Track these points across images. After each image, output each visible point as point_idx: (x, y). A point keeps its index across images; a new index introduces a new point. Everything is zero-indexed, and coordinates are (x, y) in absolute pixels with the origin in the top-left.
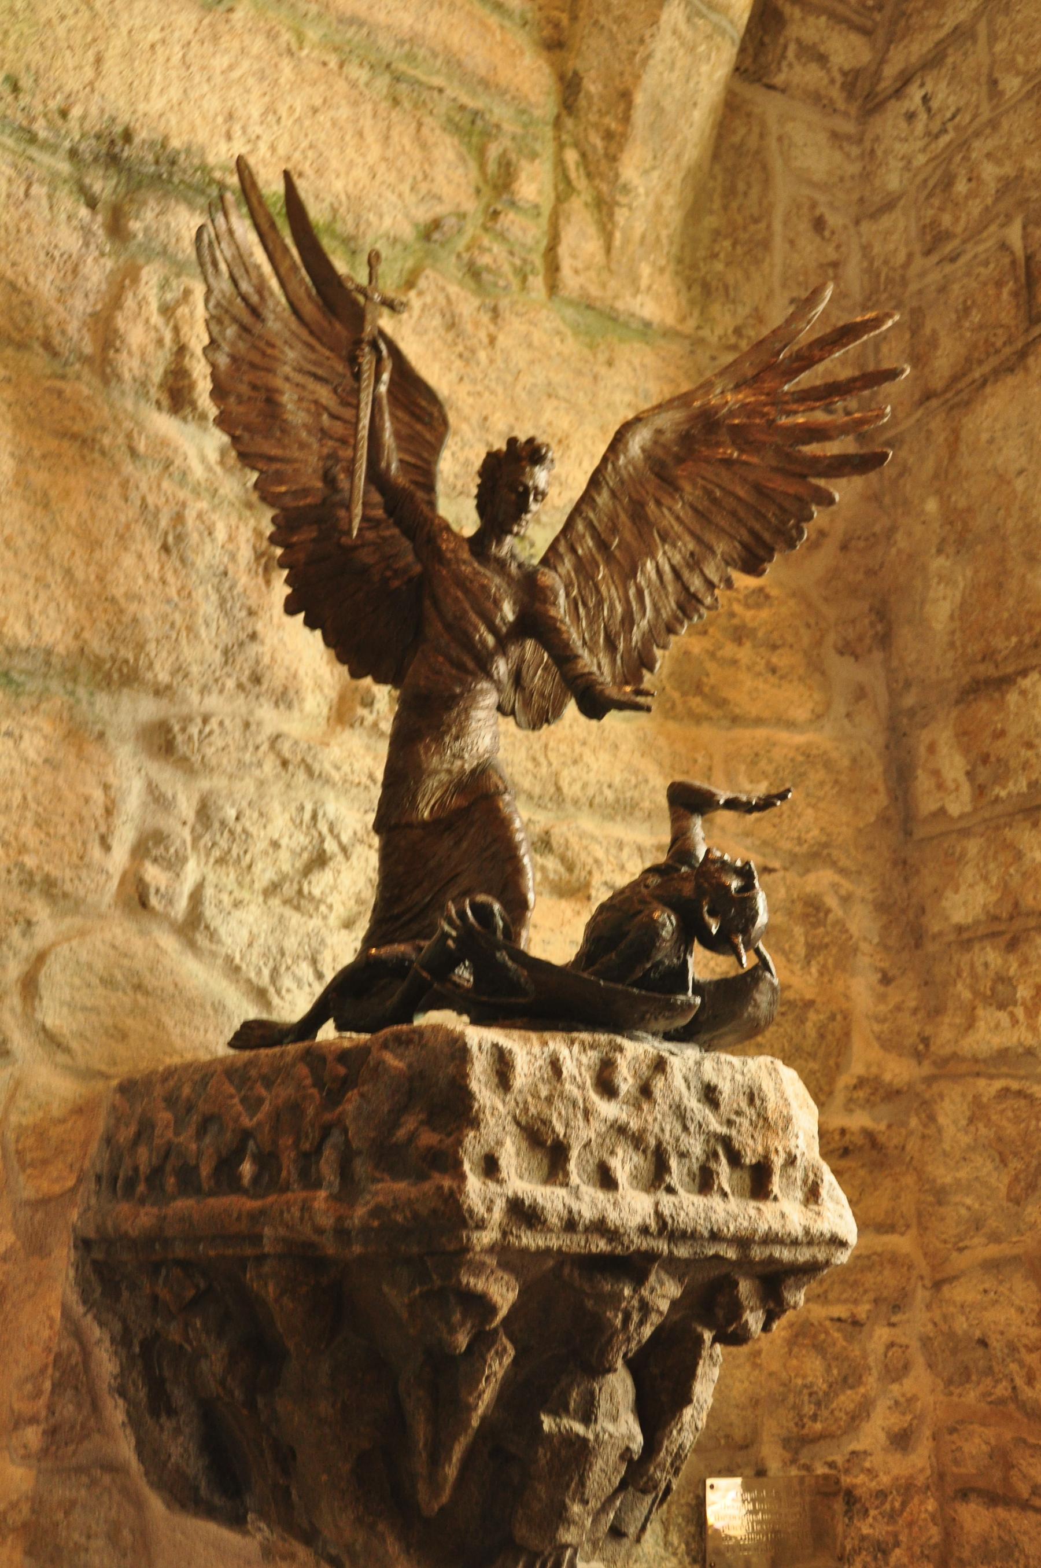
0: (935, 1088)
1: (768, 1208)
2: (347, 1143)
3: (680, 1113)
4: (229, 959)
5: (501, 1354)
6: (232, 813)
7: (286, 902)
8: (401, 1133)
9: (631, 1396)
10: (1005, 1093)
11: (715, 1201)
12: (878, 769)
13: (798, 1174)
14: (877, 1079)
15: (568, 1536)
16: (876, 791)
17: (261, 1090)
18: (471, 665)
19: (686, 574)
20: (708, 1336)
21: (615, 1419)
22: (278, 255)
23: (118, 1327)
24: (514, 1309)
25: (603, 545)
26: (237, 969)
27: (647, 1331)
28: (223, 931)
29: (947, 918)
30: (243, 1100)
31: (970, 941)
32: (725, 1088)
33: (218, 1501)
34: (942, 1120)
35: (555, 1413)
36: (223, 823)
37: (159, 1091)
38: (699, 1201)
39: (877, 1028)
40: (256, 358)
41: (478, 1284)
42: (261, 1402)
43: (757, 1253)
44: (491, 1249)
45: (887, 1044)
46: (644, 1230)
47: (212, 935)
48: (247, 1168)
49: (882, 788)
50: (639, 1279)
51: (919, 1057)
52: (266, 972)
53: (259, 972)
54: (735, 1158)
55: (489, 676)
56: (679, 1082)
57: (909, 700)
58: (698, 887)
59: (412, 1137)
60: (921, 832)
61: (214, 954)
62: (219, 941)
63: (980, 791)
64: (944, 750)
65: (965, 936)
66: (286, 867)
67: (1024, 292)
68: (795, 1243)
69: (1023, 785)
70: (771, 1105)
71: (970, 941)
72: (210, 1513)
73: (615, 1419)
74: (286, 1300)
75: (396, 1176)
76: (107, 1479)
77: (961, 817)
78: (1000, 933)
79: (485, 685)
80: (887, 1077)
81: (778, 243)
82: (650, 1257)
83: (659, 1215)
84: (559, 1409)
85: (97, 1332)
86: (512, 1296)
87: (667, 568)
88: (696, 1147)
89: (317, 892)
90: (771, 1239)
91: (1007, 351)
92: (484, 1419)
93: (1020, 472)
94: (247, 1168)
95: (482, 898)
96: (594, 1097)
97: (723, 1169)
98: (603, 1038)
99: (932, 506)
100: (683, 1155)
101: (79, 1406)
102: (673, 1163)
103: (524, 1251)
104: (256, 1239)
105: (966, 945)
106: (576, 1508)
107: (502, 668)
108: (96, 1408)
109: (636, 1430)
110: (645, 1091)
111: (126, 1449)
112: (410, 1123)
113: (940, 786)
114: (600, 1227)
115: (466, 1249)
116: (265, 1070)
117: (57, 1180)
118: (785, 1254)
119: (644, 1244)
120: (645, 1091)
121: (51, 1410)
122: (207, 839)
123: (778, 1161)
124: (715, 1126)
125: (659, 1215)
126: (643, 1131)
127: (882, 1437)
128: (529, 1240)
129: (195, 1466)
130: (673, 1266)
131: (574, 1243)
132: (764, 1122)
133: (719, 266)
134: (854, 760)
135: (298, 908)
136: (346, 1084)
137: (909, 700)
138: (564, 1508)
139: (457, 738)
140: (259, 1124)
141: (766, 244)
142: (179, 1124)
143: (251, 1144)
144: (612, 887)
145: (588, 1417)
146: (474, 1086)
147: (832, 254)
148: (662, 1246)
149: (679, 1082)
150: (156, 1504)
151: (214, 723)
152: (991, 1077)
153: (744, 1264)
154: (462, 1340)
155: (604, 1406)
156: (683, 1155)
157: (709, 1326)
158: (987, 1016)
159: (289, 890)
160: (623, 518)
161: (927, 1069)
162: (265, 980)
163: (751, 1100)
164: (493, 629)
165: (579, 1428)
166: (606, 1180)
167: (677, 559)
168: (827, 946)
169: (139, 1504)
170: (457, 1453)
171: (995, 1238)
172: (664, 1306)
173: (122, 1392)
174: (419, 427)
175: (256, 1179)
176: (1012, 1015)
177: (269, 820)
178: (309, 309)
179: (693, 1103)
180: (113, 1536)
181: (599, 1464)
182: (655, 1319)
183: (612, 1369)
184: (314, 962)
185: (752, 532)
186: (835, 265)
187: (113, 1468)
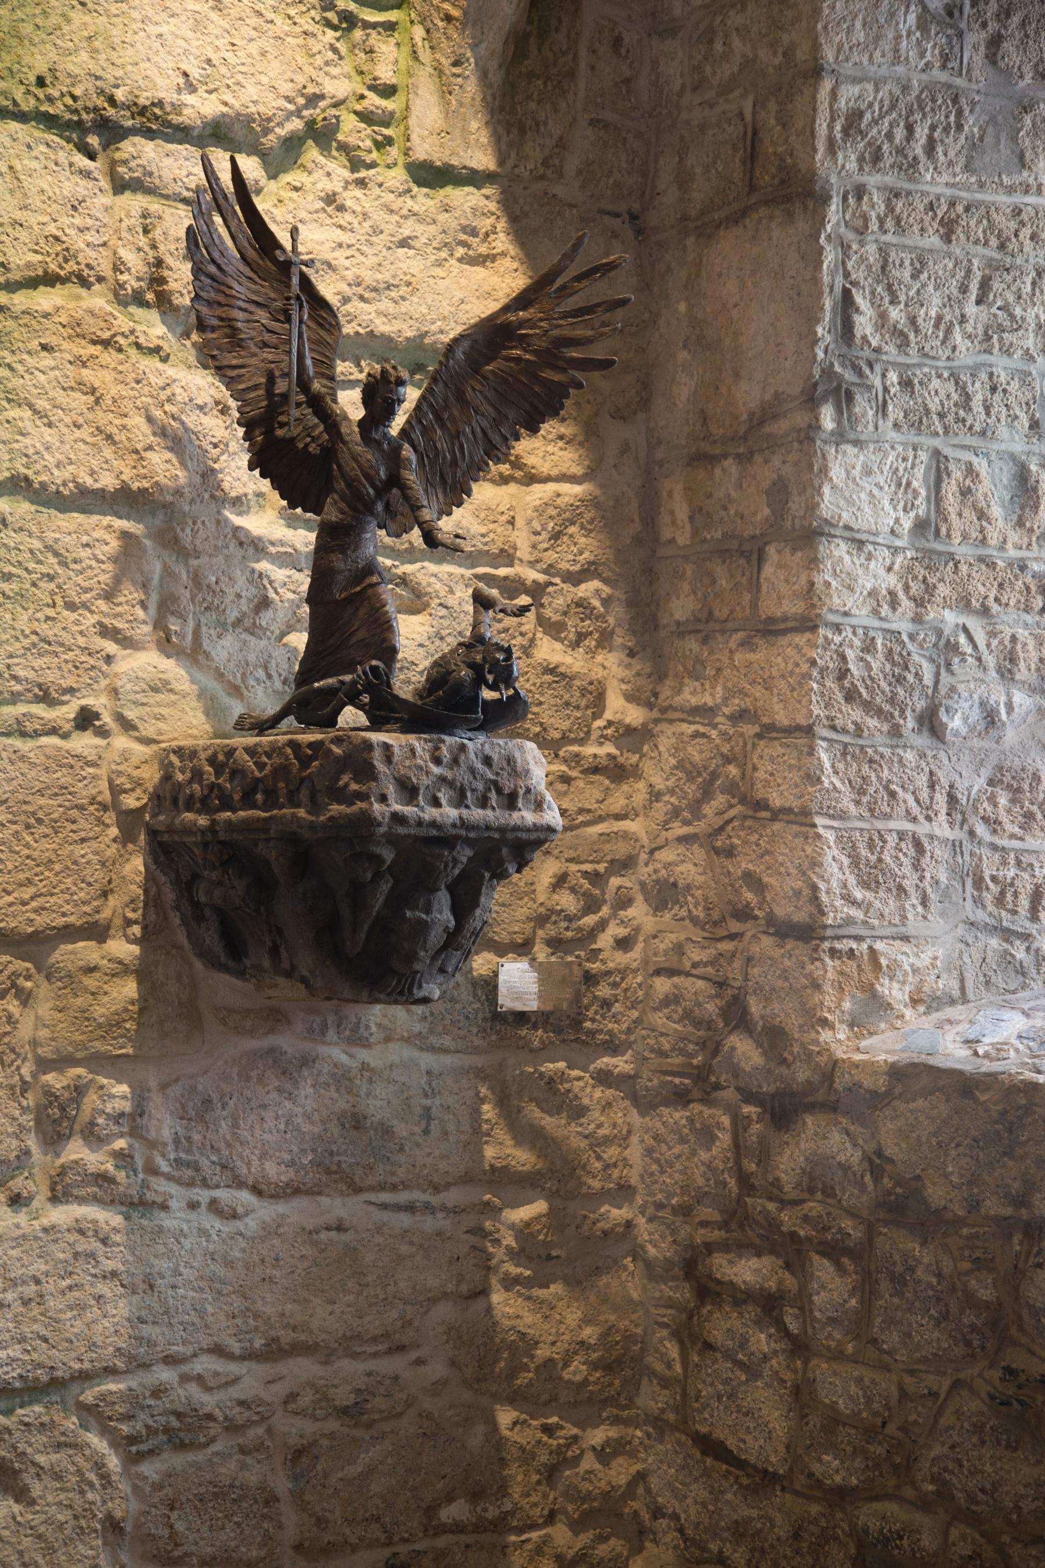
0: (659, 728)
1: (516, 815)
2: (313, 786)
3: (472, 770)
4: (217, 669)
5: (386, 882)
6: (214, 579)
7: (246, 630)
8: (341, 783)
9: (449, 902)
10: (696, 735)
11: (489, 813)
12: (635, 505)
13: (533, 798)
14: (620, 722)
15: (418, 967)
16: (633, 521)
17: (265, 759)
18: (361, 507)
19: (490, 432)
20: (487, 875)
21: (441, 913)
22: (229, 219)
23: (173, 876)
24: (393, 862)
25: (438, 418)
26: (223, 675)
27: (457, 872)
28: (213, 653)
29: (672, 615)
30: (255, 763)
31: (683, 633)
32: (495, 757)
33: (231, 964)
34: (661, 748)
35: (412, 909)
36: (208, 586)
37: (203, 756)
38: (480, 811)
39: (624, 687)
40: (222, 299)
41: (378, 850)
42: (262, 909)
43: (510, 836)
44: (384, 835)
45: (630, 698)
46: (454, 825)
47: (207, 655)
48: (259, 797)
49: (636, 518)
50: (452, 847)
51: (650, 706)
52: (239, 675)
53: (235, 676)
54: (499, 791)
55: (372, 514)
56: (472, 756)
57: (659, 455)
58: (484, 658)
59: (347, 785)
60: (663, 552)
61: (209, 668)
62: (212, 660)
63: (695, 532)
64: (677, 497)
65: (682, 629)
66: (244, 608)
67: (748, 162)
68: (528, 830)
69: (719, 534)
70: (519, 764)
71: (683, 633)
72: (227, 970)
73: (441, 913)
74: (281, 859)
75: (339, 803)
76: (174, 952)
77: (685, 547)
78: (698, 631)
79: (369, 518)
80: (628, 720)
81: (583, 69)
82: (457, 837)
83: (461, 818)
84: (415, 908)
85: (163, 879)
86: (392, 856)
87: (478, 430)
88: (480, 786)
89: (264, 623)
90: (516, 828)
91: (735, 206)
92: (378, 913)
93: (735, 306)
94: (259, 797)
95: (374, 663)
96: (431, 765)
97: (493, 795)
98: (435, 736)
99: (682, 307)
100: (473, 790)
101: (158, 915)
102: (469, 794)
103: (399, 835)
104: (267, 831)
105: (681, 635)
106: (422, 954)
107: (379, 507)
108: (166, 918)
109: (452, 918)
110: (455, 761)
111: (182, 938)
112: (345, 778)
113: (674, 522)
114: (433, 824)
115: (372, 835)
116: (267, 749)
117: (138, 799)
118: (524, 836)
119: (454, 832)
120: (455, 761)
121: (144, 915)
122: (200, 597)
123: (521, 792)
124: (490, 776)
125: (461, 818)
126: (454, 780)
127: (611, 940)
128: (401, 830)
129: (218, 948)
130: (467, 841)
131: (422, 832)
132: (515, 773)
133: (532, 105)
134: (617, 500)
135: (252, 634)
136: (312, 759)
137: (659, 455)
138: (416, 953)
139: (354, 551)
140: (265, 776)
141: (571, 74)
142: (217, 774)
143: (261, 785)
144: (408, 1011)
145: (428, 912)
146: (376, 763)
147: (627, 72)
148: (463, 833)
149: (472, 756)
150: (198, 965)
151: (199, 524)
152: (690, 723)
153: (503, 841)
154: (369, 875)
155: (436, 907)
156: (473, 790)
157: (487, 870)
158: (690, 685)
159: (247, 622)
160: (452, 399)
161: (655, 714)
162: (238, 681)
163: (509, 763)
164: (373, 486)
165: (424, 916)
166: (436, 803)
167: (485, 423)
168: (591, 633)
169: (190, 965)
170: (366, 927)
171: (687, 823)
172: (465, 860)
173: (177, 908)
174: (322, 332)
175: (265, 802)
176: (702, 685)
177: (235, 582)
178: (251, 253)
179: (479, 766)
180: (179, 978)
181: (433, 933)
182: (460, 866)
183: (439, 889)
184: (266, 668)
185: (532, 405)
186: (627, 81)
187: (180, 948)
